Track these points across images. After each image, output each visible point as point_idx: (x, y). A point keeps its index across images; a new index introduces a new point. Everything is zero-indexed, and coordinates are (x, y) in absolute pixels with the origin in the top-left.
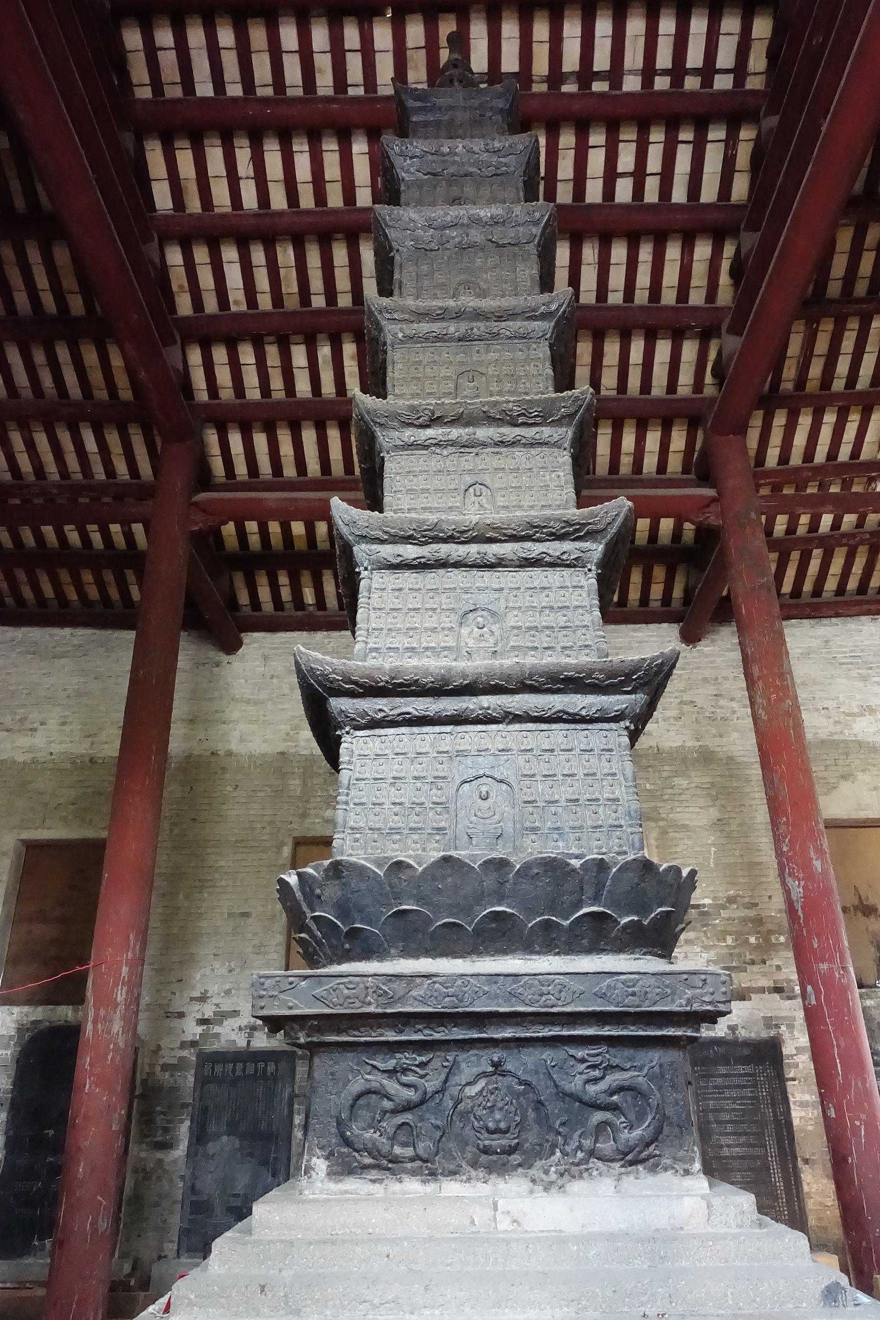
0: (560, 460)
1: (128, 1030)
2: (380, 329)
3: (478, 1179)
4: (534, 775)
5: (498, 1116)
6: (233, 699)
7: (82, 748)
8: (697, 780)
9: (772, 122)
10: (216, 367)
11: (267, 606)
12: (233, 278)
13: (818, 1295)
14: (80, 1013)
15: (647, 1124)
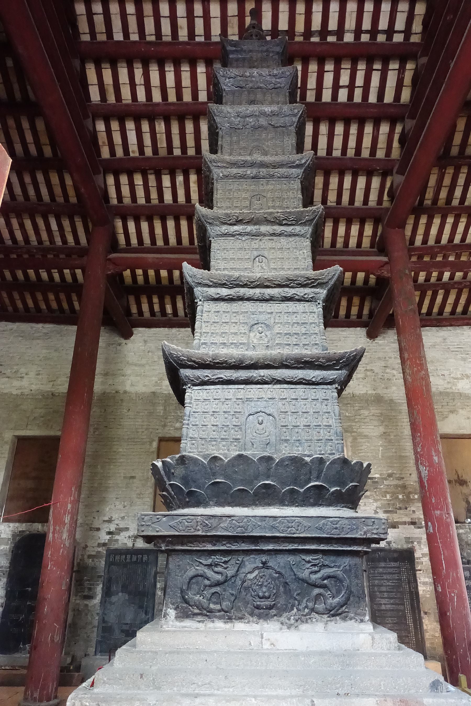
0: (305, 244)
1: (71, 537)
2: (210, 171)
3: (253, 622)
4: (287, 412)
5: (264, 589)
6: (128, 363)
7: (48, 388)
8: (373, 411)
9: (424, 60)
10: (122, 186)
11: (147, 314)
12: (132, 138)
13: (428, 685)
14: (45, 527)
15: (341, 596)
